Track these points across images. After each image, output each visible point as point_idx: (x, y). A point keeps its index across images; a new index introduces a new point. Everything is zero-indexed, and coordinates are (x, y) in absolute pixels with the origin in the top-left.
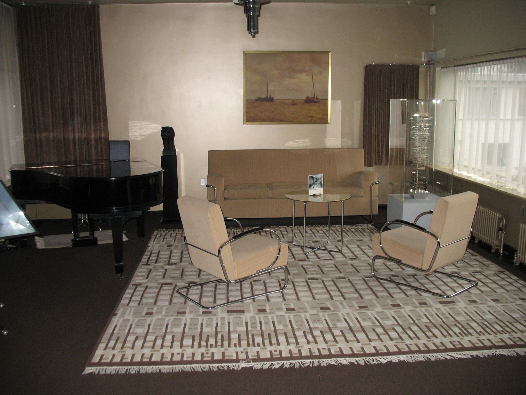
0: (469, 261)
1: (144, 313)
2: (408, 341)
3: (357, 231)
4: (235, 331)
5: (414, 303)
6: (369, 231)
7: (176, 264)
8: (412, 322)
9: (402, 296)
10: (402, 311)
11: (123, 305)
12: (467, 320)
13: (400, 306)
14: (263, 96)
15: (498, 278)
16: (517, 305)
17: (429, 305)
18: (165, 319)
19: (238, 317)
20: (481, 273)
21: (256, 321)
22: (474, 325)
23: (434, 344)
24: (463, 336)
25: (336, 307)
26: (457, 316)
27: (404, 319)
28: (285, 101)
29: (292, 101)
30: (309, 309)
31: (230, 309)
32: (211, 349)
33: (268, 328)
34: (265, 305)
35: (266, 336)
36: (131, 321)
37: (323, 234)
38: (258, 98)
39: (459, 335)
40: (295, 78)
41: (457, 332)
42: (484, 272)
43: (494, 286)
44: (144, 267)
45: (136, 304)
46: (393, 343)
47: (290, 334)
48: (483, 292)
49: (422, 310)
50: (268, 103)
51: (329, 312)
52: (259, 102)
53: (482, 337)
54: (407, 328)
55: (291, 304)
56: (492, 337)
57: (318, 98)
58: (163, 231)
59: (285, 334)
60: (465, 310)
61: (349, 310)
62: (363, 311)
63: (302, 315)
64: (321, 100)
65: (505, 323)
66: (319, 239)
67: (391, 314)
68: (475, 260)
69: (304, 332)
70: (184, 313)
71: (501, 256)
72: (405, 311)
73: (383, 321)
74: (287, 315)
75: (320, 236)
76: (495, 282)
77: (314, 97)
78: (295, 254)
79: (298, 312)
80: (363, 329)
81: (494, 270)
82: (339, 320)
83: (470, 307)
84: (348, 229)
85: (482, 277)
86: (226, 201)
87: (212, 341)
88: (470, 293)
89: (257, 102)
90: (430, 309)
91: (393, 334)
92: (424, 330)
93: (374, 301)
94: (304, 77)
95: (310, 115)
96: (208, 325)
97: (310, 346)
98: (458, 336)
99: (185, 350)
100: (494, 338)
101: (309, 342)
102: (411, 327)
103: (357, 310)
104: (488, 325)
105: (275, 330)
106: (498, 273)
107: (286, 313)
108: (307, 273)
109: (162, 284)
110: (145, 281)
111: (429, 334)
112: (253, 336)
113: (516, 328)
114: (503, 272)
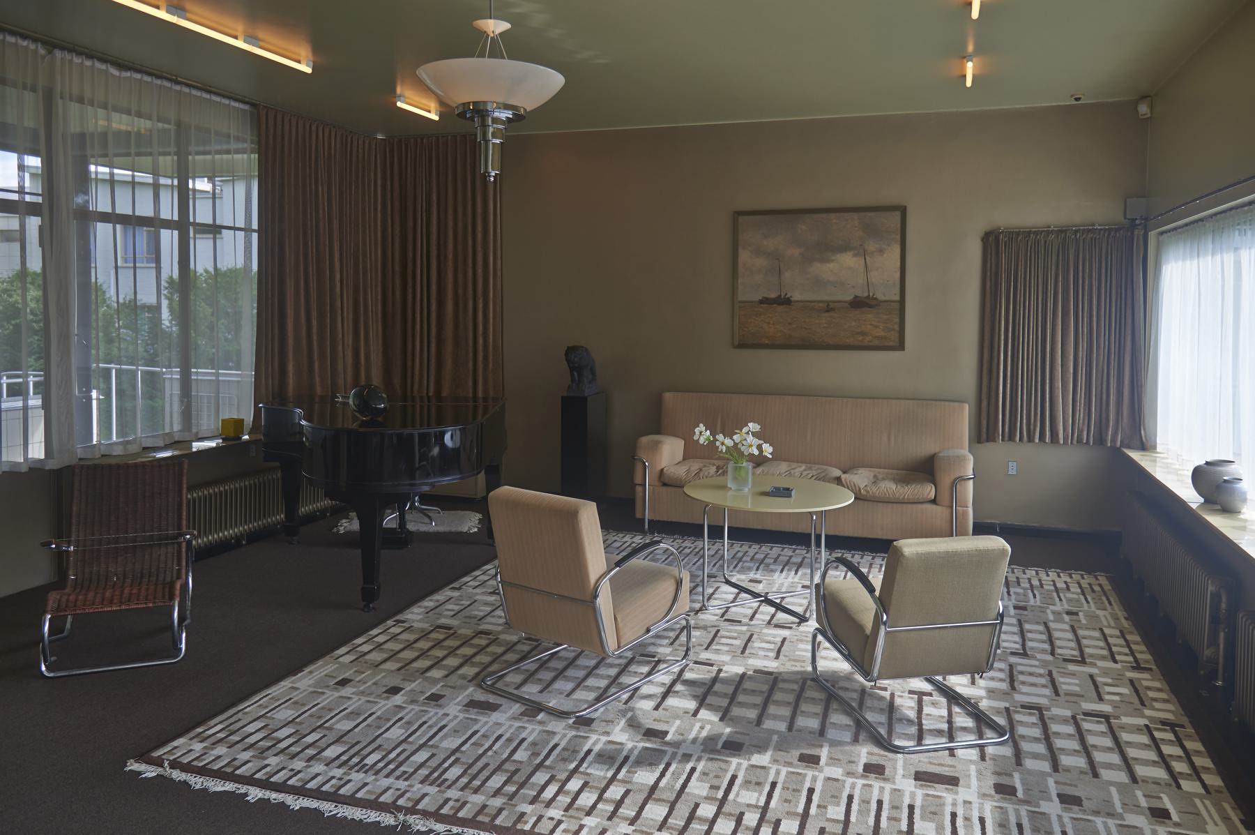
7: (790, 628)
14: (773, 295)
18: (806, 774)
19: (1085, 820)
28: (813, 304)
36: (504, 728)
37: (1078, 594)
38: (764, 298)
40: (832, 261)
50: (780, 308)
51: (1076, 812)
52: (765, 305)
57: (876, 299)
58: (739, 545)
64: (881, 302)
67: (1018, 816)
71: (69, 583)
78: (1072, 641)
86: (665, 489)
89: (762, 305)
94: (848, 260)
95: (859, 331)
112: (457, 760)
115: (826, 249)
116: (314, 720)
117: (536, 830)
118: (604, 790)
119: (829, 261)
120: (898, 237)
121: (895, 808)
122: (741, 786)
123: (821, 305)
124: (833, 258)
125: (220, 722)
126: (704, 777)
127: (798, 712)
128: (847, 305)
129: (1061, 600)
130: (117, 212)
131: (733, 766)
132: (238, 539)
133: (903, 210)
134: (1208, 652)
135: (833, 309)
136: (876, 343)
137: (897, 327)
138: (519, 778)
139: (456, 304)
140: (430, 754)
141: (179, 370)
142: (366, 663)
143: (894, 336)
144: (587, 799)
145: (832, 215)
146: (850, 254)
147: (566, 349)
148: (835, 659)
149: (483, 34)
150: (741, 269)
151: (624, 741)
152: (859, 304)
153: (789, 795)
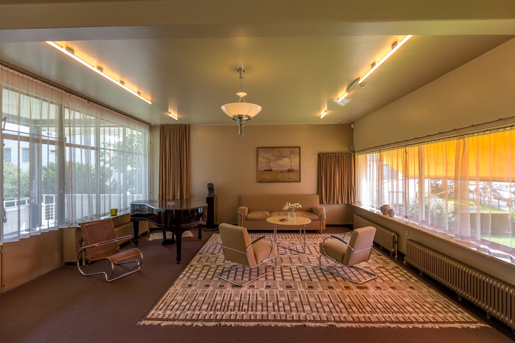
0: (377, 259)
2: (335, 314)
3: (315, 238)
4: (293, 301)
5: (341, 287)
6: (321, 238)
8: (340, 301)
9: (334, 280)
10: (334, 291)
11: (180, 279)
12: (375, 302)
13: (333, 288)
14: (268, 169)
15: (394, 271)
16: (407, 292)
17: (351, 289)
20: (384, 268)
21: (315, 294)
22: (379, 305)
23: (352, 317)
24: (373, 314)
25: (296, 286)
26: (404, 298)
29: (281, 171)
30: (279, 287)
33: (253, 300)
34: (269, 283)
35: (250, 305)
40: (282, 160)
42: (385, 267)
43: (391, 277)
44: (199, 255)
45: (202, 279)
46: (326, 315)
47: (265, 304)
48: (384, 281)
49: (346, 292)
50: (269, 172)
51: (291, 290)
53: (385, 315)
54: (336, 305)
55: (270, 283)
56: (391, 315)
59: (262, 304)
60: (300, 293)
61: (303, 290)
62: (311, 290)
63: (275, 291)
65: (383, 305)
66: (294, 242)
68: (381, 258)
69: (273, 304)
72: (336, 292)
73: (322, 298)
74: (265, 291)
75: (295, 241)
76: (391, 274)
77: (292, 169)
79: (272, 289)
80: (309, 304)
82: (296, 296)
83: (385, 292)
84: (311, 237)
85: (384, 270)
87: (218, 307)
88: (376, 281)
90: (351, 291)
91: (327, 309)
92: (347, 307)
93: (318, 283)
94: (286, 160)
96: (220, 295)
97: (275, 313)
98: (369, 313)
99: (202, 312)
100: (392, 316)
101: (274, 311)
102: (339, 304)
103: (307, 289)
104: (388, 306)
105: (257, 301)
106: (395, 268)
107: (265, 289)
108: (282, 262)
109: (204, 266)
111: (350, 310)
114: (398, 267)
115: (281, 157)
118: (192, 304)
119: (282, 160)
120: (299, 154)
123: (280, 171)
124: (283, 159)
125: (161, 304)
126: (260, 296)
127: (251, 275)
128: (286, 171)
129: (310, 241)
130: (47, 145)
131: (224, 291)
133: (300, 148)
134: (393, 250)
135: (283, 172)
136: (294, 180)
137: (299, 176)
138: (167, 304)
140: (187, 302)
141: (95, 195)
142: (180, 279)
144: (176, 307)
146: (287, 158)
147: (207, 184)
148: (379, 262)
149: (239, 97)
150: (259, 162)
152: (289, 171)
153: (271, 296)
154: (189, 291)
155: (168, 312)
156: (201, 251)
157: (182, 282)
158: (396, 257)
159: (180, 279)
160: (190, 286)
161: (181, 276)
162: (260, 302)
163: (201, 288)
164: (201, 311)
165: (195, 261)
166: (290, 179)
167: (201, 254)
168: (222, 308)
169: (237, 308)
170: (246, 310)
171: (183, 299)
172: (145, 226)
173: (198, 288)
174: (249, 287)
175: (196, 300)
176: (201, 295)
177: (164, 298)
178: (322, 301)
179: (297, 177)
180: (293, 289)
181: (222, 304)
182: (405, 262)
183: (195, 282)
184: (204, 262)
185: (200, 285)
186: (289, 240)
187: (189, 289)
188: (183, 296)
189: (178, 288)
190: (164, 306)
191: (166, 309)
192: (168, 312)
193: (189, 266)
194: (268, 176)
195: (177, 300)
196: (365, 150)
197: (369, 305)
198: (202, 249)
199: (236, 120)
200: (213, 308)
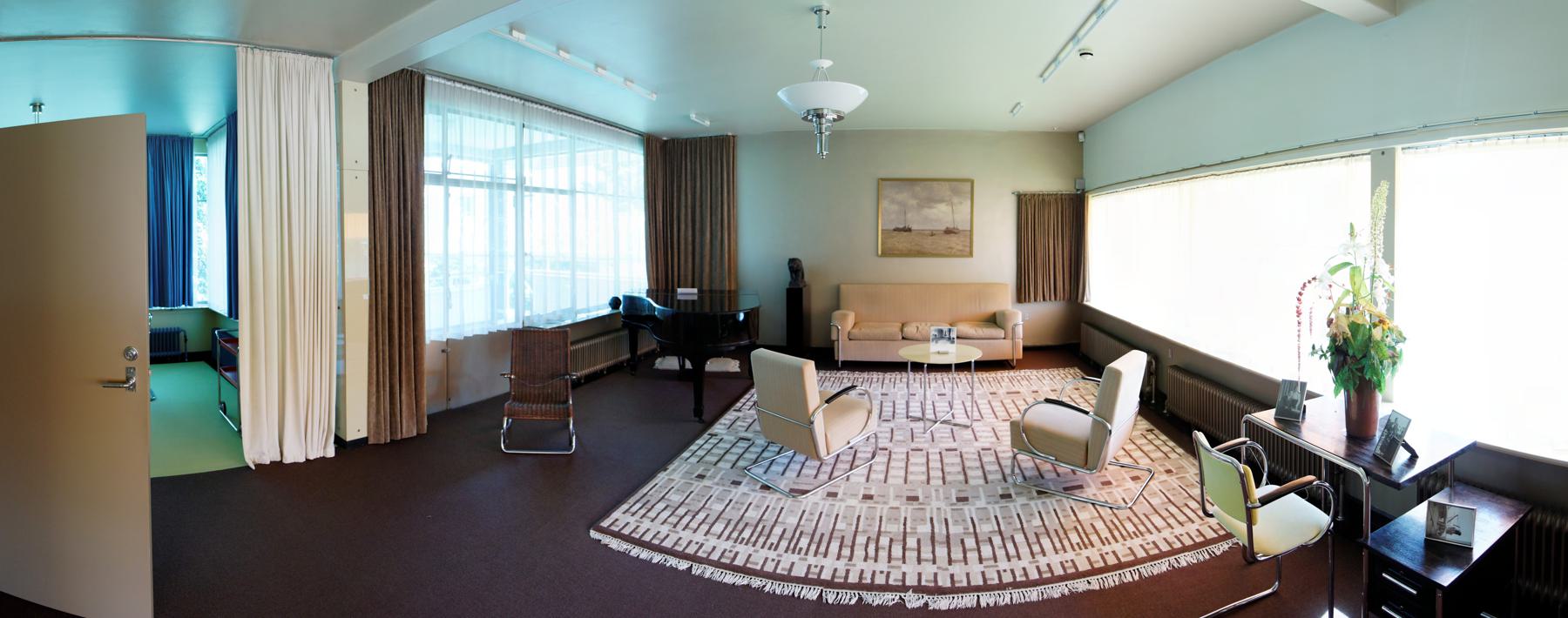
1: (696, 474)
11: (682, 459)
14: (901, 226)
27: (1010, 520)
31: (824, 538)
32: (739, 546)
39: (1076, 547)
41: (1074, 542)
50: (905, 234)
51: (915, 505)
55: (874, 488)
61: (942, 505)
69: (869, 538)
70: (739, 483)
74: (859, 506)
81: (1141, 430)
107: (860, 502)
110: (725, 432)
113: (1153, 524)
114: (1151, 431)
115: (931, 201)
116: (657, 493)
117: (622, 532)
119: (930, 207)
121: (811, 514)
122: (887, 522)
132: (602, 371)
136: (959, 253)
139: (711, 234)
143: (968, 249)
145: (935, 183)
151: (898, 506)
152: (948, 232)
154: (698, 486)
155: (646, 524)
156: (739, 405)
157: (685, 467)
158: (1153, 402)
159: (682, 459)
160: (701, 477)
161: (686, 454)
162: (840, 535)
163: (723, 485)
164: (708, 536)
165: (723, 427)
166: (950, 250)
167: (739, 410)
168: (753, 539)
169: (784, 544)
170: (803, 551)
171: (681, 501)
172: (648, 343)
173: (717, 484)
174: (825, 496)
175: (707, 509)
176: (720, 500)
177: (644, 490)
178: (978, 531)
179: (964, 246)
180: (920, 504)
181: (756, 526)
182: (1165, 412)
183: (713, 470)
184: (742, 431)
185: (721, 479)
186: (935, 387)
187: (696, 483)
188: (683, 496)
189: (676, 476)
190: (640, 508)
191: (644, 516)
192: (646, 524)
193: (706, 436)
194: (901, 241)
195: (670, 500)
196: (1141, 181)
197: (1079, 528)
198: (743, 400)
199: (811, 120)
200: (735, 535)
